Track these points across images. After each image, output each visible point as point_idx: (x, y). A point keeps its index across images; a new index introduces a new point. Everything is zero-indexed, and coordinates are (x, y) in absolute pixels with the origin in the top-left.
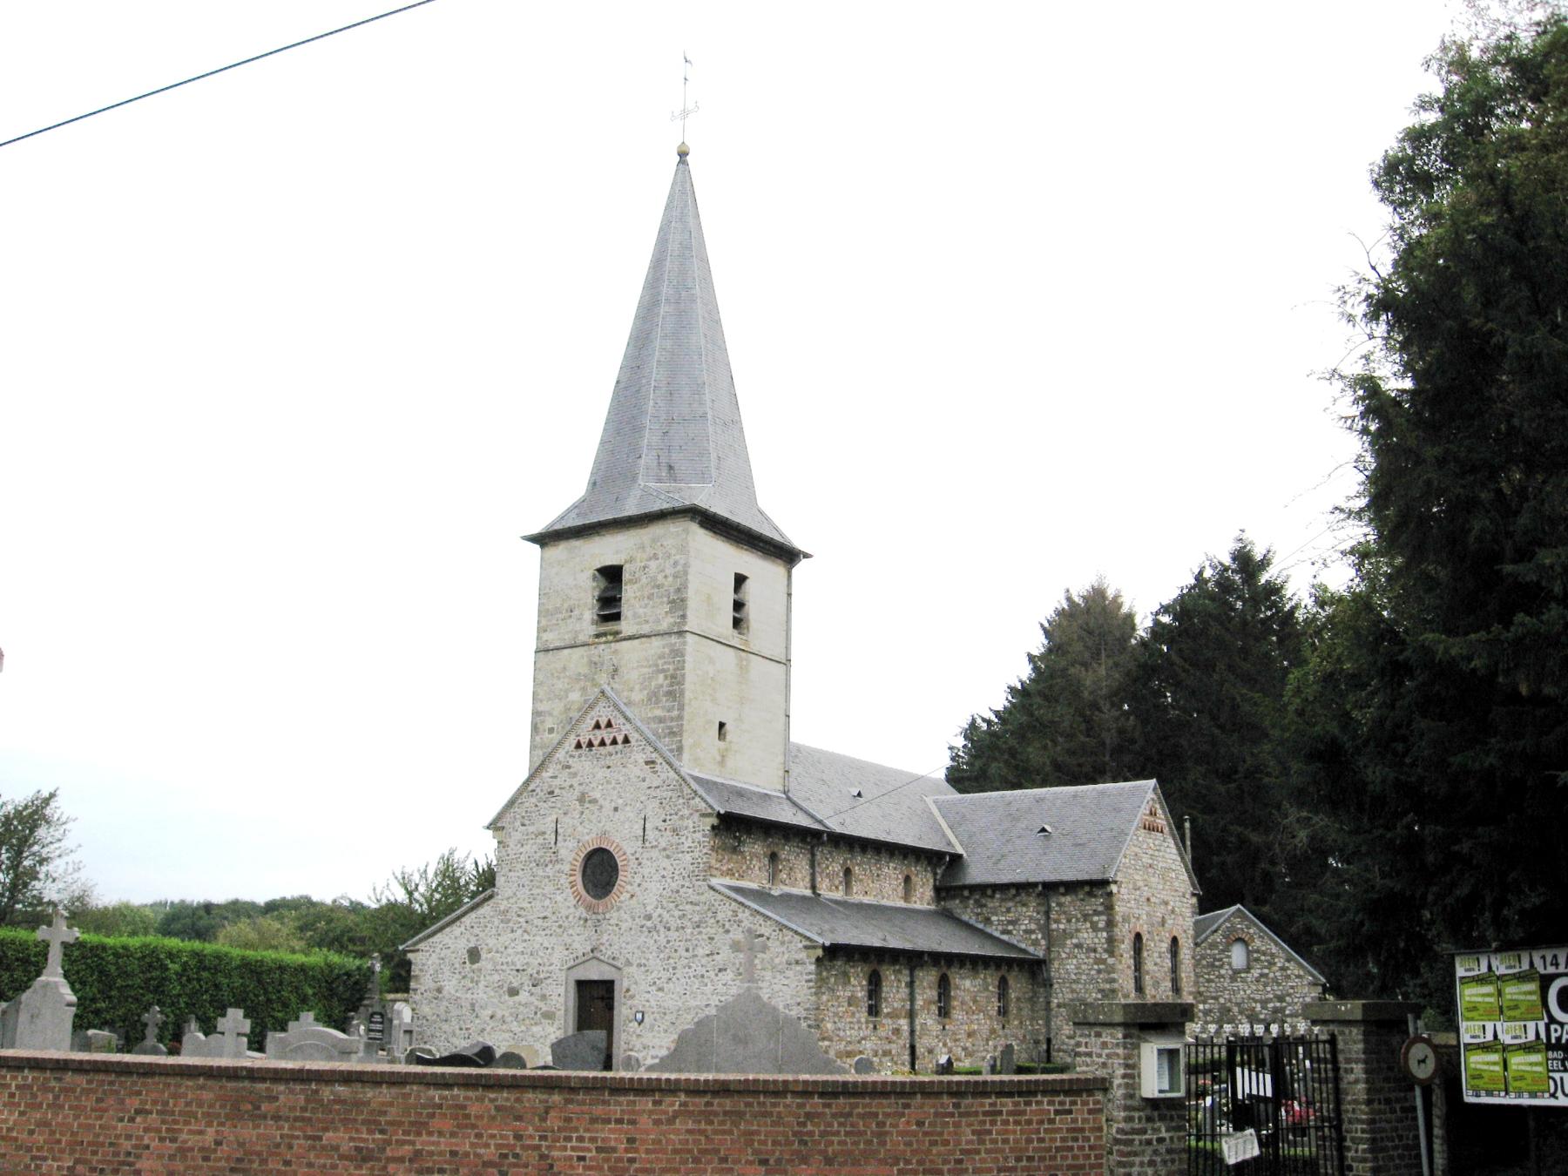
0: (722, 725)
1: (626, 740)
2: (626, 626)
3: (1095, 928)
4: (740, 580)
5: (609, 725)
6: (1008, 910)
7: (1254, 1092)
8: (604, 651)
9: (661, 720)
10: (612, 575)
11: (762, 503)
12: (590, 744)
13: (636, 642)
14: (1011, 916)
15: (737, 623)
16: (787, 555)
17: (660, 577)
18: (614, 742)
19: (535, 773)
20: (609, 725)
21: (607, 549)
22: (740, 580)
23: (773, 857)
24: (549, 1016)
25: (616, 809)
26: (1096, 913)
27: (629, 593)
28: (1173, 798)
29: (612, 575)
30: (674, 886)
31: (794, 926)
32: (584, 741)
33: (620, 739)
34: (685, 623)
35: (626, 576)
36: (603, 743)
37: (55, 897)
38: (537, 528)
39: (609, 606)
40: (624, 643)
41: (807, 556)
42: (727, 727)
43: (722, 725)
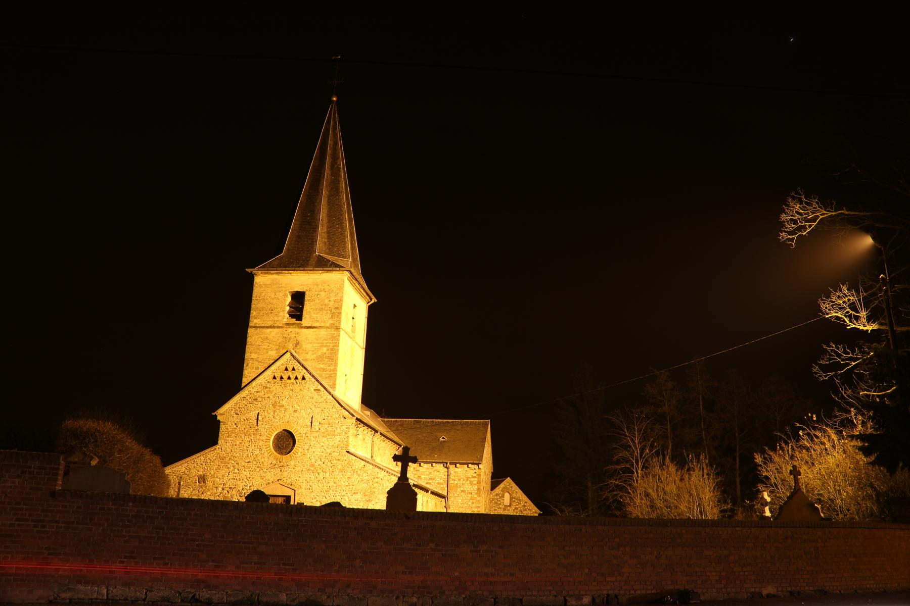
1: (303, 378)
2: (305, 321)
3: (471, 483)
5: (294, 369)
6: (430, 473)
8: (293, 330)
9: (324, 370)
12: (282, 378)
13: (310, 330)
14: (431, 476)
17: (326, 301)
20: (294, 369)
25: (295, 411)
26: (473, 477)
27: (308, 307)
28: (770, 442)
29: (298, 298)
30: (329, 451)
32: (278, 375)
33: (300, 377)
35: (307, 298)
36: (289, 378)
37: (716, 510)
40: (304, 330)
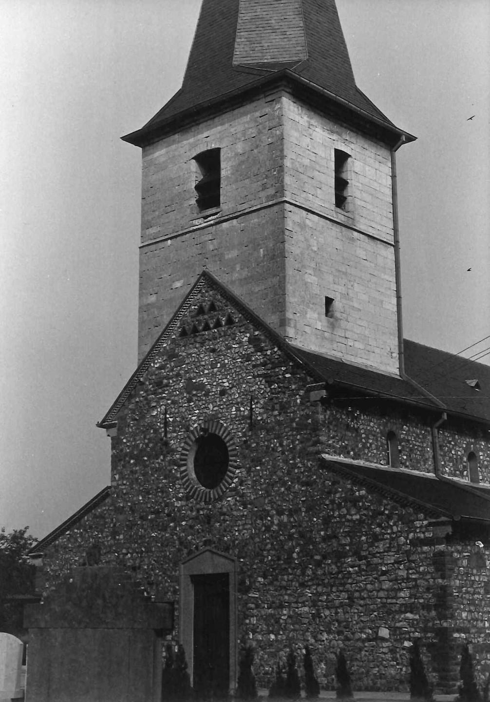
0: (329, 301)
4: (341, 158)
5: (213, 307)
7: (217, 433)
10: (209, 161)
11: (361, 83)
15: (340, 201)
16: (386, 136)
18: (218, 324)
19: (144, 365)
21: (206, 138)
22: (341, 158)
23: (391, 436)
24: (472, 456)
29: (209, 161)
31: (254, 219)
33: (224, 320)
34: (283, 196)
36: (207, 328)
38: (138, 125)
39: (209, 194)
41: (411, 138)
42: (337, 305)
43: (329, 301)
